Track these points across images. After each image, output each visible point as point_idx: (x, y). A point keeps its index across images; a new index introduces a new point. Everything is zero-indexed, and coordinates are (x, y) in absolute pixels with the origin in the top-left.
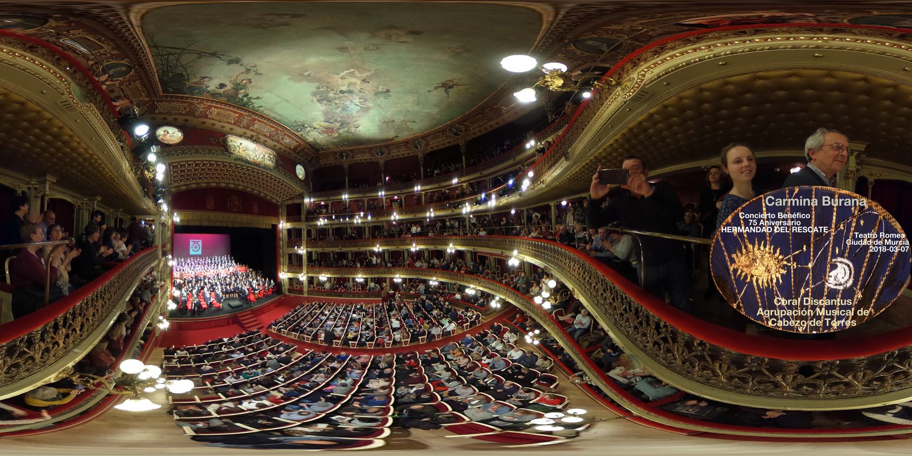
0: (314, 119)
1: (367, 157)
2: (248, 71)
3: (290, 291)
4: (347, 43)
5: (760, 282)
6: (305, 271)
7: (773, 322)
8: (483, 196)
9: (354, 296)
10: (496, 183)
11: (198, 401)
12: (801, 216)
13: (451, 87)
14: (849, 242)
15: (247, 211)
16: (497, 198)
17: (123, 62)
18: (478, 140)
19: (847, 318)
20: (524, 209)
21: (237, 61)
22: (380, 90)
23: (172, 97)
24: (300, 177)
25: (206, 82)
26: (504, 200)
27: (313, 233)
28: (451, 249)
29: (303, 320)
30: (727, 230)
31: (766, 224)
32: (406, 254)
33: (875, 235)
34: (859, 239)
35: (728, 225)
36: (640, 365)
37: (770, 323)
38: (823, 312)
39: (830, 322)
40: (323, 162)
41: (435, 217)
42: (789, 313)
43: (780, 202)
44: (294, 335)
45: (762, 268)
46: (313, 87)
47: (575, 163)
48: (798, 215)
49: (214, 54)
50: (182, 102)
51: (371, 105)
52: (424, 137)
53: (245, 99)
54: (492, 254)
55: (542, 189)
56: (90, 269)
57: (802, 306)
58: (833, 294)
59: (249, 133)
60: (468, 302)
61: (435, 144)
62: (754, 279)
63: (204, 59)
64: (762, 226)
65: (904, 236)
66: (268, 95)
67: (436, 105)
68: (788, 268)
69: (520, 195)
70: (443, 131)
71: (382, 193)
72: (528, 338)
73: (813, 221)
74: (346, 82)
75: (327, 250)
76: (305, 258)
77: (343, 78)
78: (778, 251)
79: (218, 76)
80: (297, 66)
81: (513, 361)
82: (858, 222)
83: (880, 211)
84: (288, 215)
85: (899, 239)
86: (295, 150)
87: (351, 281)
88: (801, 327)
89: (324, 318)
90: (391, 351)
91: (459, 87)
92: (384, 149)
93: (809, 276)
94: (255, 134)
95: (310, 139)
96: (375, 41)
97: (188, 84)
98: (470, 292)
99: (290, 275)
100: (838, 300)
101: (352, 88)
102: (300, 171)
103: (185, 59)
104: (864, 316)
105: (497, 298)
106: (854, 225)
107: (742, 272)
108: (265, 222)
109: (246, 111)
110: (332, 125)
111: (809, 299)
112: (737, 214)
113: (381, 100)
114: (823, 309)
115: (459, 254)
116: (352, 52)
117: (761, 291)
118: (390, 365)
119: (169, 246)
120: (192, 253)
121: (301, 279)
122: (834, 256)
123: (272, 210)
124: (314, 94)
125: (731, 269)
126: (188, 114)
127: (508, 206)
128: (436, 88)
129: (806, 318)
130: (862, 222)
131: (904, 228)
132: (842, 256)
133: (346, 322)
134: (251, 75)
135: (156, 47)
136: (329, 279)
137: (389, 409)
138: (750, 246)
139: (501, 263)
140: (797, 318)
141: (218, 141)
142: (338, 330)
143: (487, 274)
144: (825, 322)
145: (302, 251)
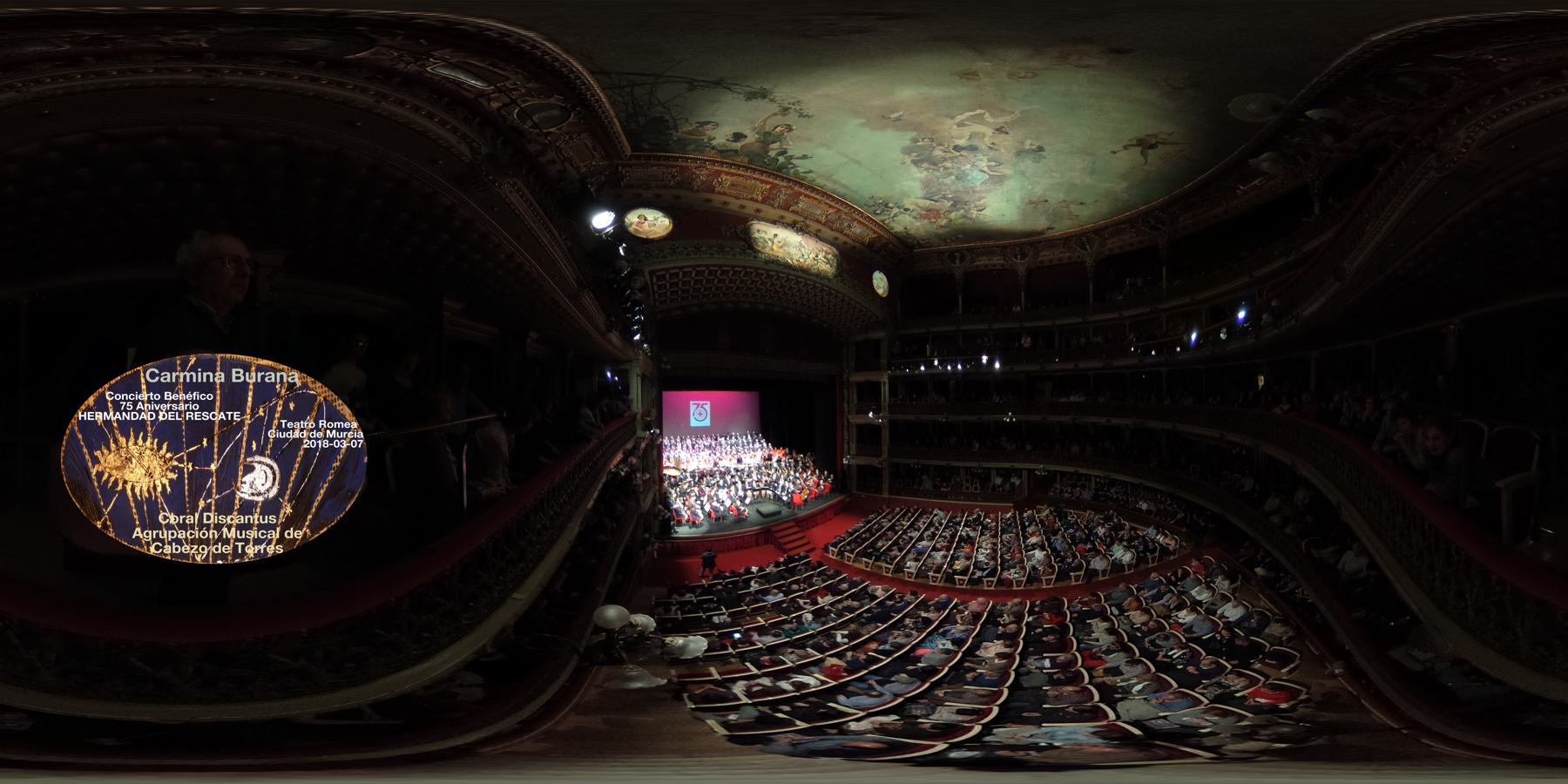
0: (905, 195)
1: (997, 260)
2: (785, 111)
5: (137, 491)
7: (157, 548)
11: (717, 676)
12: (201, 397)
13: (1152, 147)
14: (272, 434)
17: (552, 101)
21: (763, 95)
23: (649, 157)
24: (880, 291)
25: (709, 131)
30: (88, 416)
31: (146, 406)
33: (311, 424)
34: (287, 430)
35: (89, 409)
37: (152, 549)
38: (232, 534)
42: (182, 535)
43: (167, 377)
44: (864, 564)
45: (140, 471)
46: (905, 139)
49: (718, 83)
50: (667, 167)
51: (1008, 172)
53: (781, 159)
57: (201, 525)
58: (247, 507)
59: (790, 217)
62: (129, 487)
64: (140, 411)
65: (355, 425)
66: (822, 151)
68: (181, 471)
70: (1131, 222)
74: (967, 131)
79: (730, 121)
80: (877, 102)
82: (286, 406)
83: (319, 390)
86: (871, 245)
88: (200, 555)
89: (916, 534)
90: (1024, 594)
95: (898, 228)
97: (675, 135)
101: (975, 142)
102: (880, 282)
109: (783, 179)
112: (103, 394)
113: (1028, 164)
116: (985, 80)
117: (139, 504)
118: (1019, 618)
120: (693, 423)
122: (249, 453)
124: (907, 151)
125: (94, 472)
128: (1125, 148)
129: (207, 542)
130: (292, 406)
132: (262, 454)
133: (951, 542)
134: (791, 119)
137: (1001, 693)
138: (122, 440)
140: (193, 542)
141: (733, 231)
142: (938, 556)
144: (235, 548)
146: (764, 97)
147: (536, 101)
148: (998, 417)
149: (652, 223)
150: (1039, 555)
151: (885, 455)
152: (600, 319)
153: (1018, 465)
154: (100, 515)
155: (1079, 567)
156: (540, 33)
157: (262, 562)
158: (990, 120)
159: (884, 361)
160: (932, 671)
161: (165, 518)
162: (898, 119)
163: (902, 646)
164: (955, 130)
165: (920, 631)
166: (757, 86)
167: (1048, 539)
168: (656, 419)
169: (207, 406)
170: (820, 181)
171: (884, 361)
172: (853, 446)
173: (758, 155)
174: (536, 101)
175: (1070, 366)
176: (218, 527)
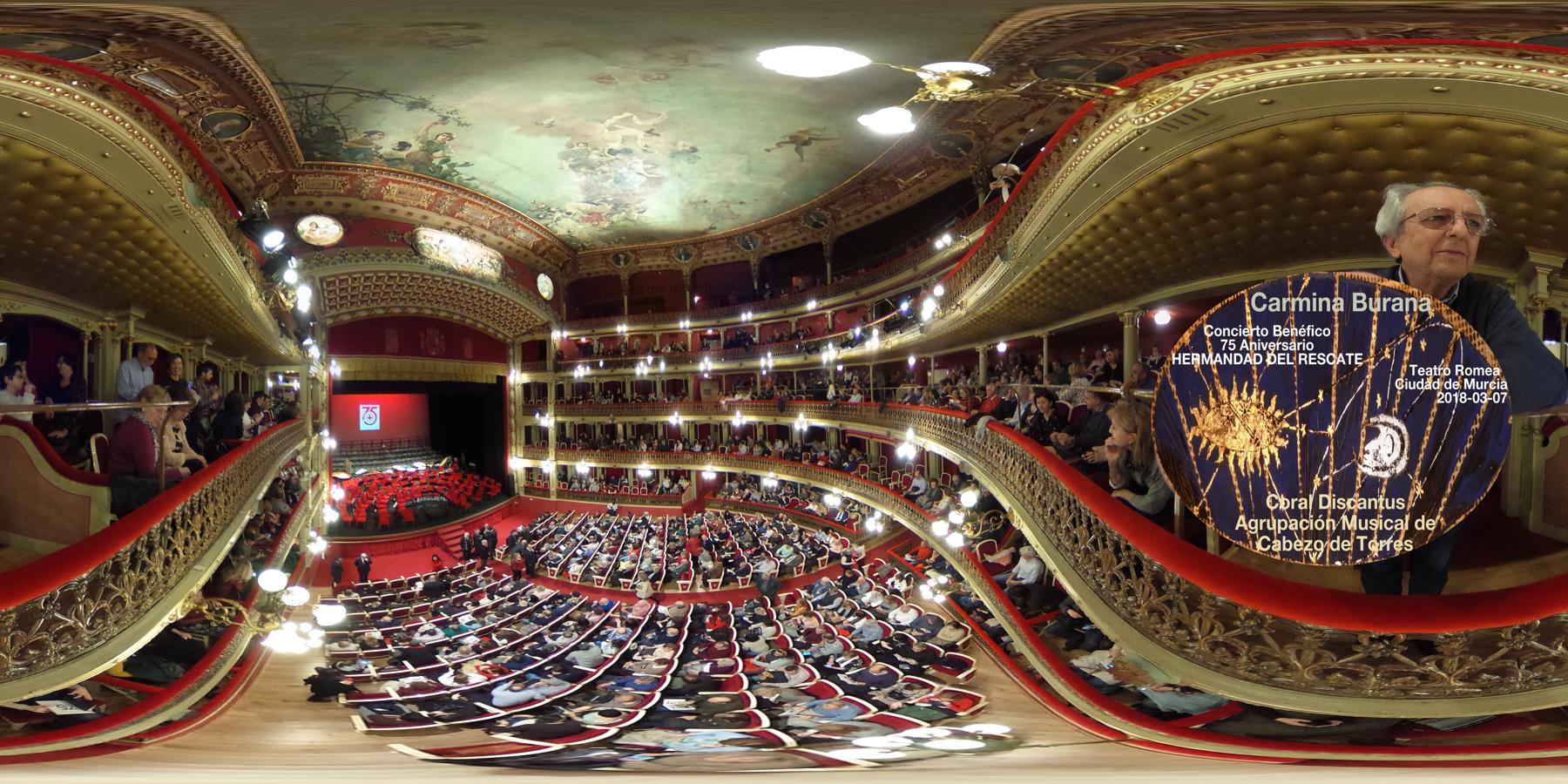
1: (660, 262)
2: (445, 120)
3: (528, 490)
4: (609, 69)
5: (1241, 463)
6: (552, 456)
7: (1265, 544)
8: (858, 331)
9: (634, 502)
10: (883, 309)
13: (806, 143)
14: (1400, 384)
15: (453, 353)
16: (881, 336)
17: (235, 110)
18: (852, 235)
20: (932, 356)
21: (423, 104)
22: (680, 147)
23: (320, 167)
26: (895, 340)
27: (567, 391)
28: (802, 422)
30: (1183, 359)
31: (1255, 348)
32: (725, 431)
33: (1445, 370)
34: (1417, 378)
35: (1184, 349)
36: (1123, 648)
38: (1352, 524)
39: (1366, 542)
40: (586, 270)
41: (776, 367)
42: (1293, 525)
46: (560, 144)
47: (1019, 266)
48: (1310, 330)
49: (381, 94)
52: (760, 230)
53: (445, 167)
54: (872, 436)
55: (959, 319)
56: (217, 436)
57: (1317, 512)
58: (1371, 487)
59: (455, 223)
60: (827, 522)
61: (781, 242)
62: (1231, 459)
63: (365, 103)
64: (1244, 352)
65: (1498, 371)
67: (779, 175)
68: (1290, 435)
69: (922, 330)
70: (793, 220)
71: (685, 324)
72: (925, 591)
73: (1336, 342)
74: (618, 135)
75: (590, 420)
76: (552, 435)
77: (611, 128)
78: (1273, 402)
79: (394, 130)
80: (528, 109)
81: (899, 627)
82: (1416, 345)
84: (524, 361)
85: (1490, 378)
86: (535, 249)
87: (630, 474)
91: (821, 144)
92: (691, 249)
93: (1329, 451)
98: (833, 500)
99: (529, 463)
100: (1381, 499)
101: (629, 146)
102: (545, 285)
103: (335, 103)
104: (1427, 532)
105: (878, 515)
106: (1409, 349)
107: (1209, 443)
108: (485, 373)
109: (447, 186)
111: (1328, 497)
112: (1201, 328)
113: (683, 165)
114: (1354, 517)
115: (816, 434)
116: (622, 84)
117: (1243, 482)
119: (324, 416)
121: (546, 471)
122: (1374, 411)
123: (495, 351)
124: (565, 156)
126: (349, 194)
127: (902, 351)
128: (779, 145)
129: (1322, 535)
130: (1423, 344)
131: (1497, 356)
132: (1388, 412)
134: (451, 127)
136: (594, 471)
138: (1223, 392)
139: (887, 450)
140: (1307, 535)
141: (402, 236)
143: (864, 470)
144: (1357, 542)
145: (548, 421)
147: (221, 110)
153: (687, 467)
154: (1198, 497)
158: (639, 122)
161: (1275, 501)
162: (551, 125)
164: (607, 134)
169: (1323, 345)
170: (483, 188)
174: (221, 110)
176: (1337, 514)
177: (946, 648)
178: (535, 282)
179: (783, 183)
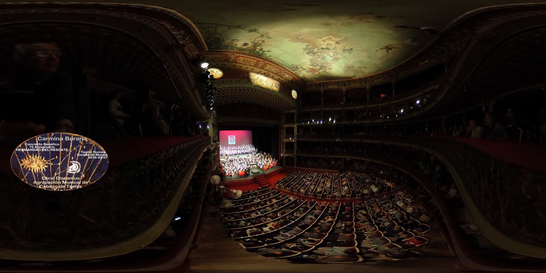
0: (304, 64)
1: (336, 87)
2: (262, 36)
5: (35, 171)
9: (323, 169)
13: (390, 49)
14: (78, 155)
19: (77, 185)
21: (255, 30)
22: (347, 48)
23: (214, 51)
29: (293, 181)
30: (19, 150)
33: (91, 152)
35: (19, 148)
42: (49, 183)
43: (44, 139)
46: (304, 45)
49: (239, 27)
52: (371, 77)
53: (261, 52)
58: (70, 175)
59: (263, 71)
65: (105, 152)
67: (380, 59)
68: (49, 165)
70: (383, 74)
74: (326, 43)
79: (243, 39)
80: (295, 33)
83: (93, 143)
86: (291, 81)
94: (266, 72)
96: (352, 21)
101: (329, 47)
102: (294, 94)
103: (220, 30)
109: (261, 58)
110: (315, 68)
113: (347, 54)
122: (71, 160)
124: (305, 49)
128: (381, 49)
129: (57, 185)
132: (75, 160)
134: (264, 38)
135: (200, 24)
138: (30, 157)
140: (53, 185)
142: (312, 187)
144: (66, 186)
146: (255, 31)
148: (334, 140)
149: (217, 73)
150: (346, 188)
151: (295, 153)
152: (200, 101)
155: (359, 192)
156: (176, 10)
157: (75, 190)
159: (295, 120)
160: (307, 226)
162: (302, 39)
163: (298, 217)
165: (304, 212)
166: (252, 28)
167: (293, 203)
168: (217, 140)
169: (58, 147)
170: (274, 59)
171: (295, 120)
172: (284, 150)
173: (252, 50)
175: (359, 122)
177: (422, 222)
178: (291, 93)
179: (381, 62)
